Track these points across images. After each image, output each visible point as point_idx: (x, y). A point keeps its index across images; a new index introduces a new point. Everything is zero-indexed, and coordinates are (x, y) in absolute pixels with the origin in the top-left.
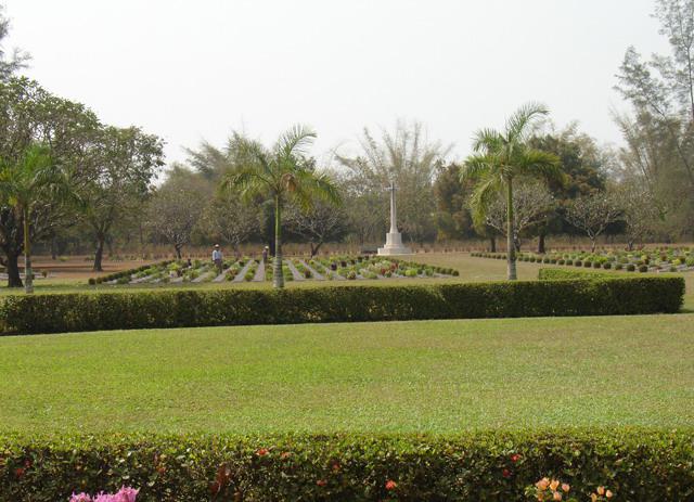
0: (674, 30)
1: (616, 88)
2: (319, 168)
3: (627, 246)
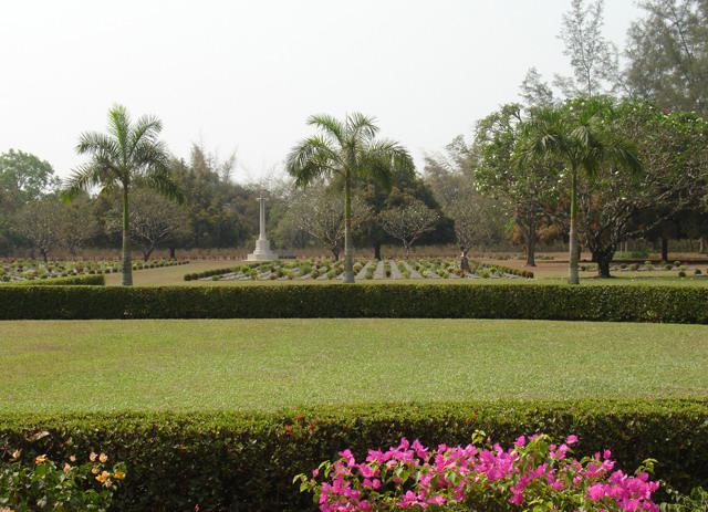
0: (577, 52)
1: (520, 95)
2: (420, 168)
3: (598, 455)
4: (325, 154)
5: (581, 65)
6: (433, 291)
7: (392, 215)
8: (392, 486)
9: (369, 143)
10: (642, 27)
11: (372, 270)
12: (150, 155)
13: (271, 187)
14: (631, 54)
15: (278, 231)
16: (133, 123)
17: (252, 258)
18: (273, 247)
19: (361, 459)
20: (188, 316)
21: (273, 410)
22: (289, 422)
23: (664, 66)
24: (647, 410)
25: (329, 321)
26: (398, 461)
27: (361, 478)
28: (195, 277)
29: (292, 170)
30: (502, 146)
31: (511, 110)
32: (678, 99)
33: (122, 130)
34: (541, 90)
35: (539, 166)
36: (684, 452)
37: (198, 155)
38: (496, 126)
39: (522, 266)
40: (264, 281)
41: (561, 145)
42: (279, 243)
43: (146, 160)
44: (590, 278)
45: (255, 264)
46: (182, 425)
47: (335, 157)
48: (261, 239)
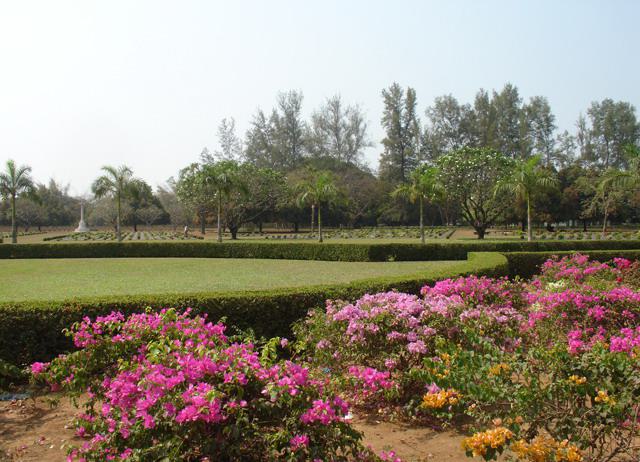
2: (155, 191)
4: (109, 183)
5: (226, 147)
6: (156, 246)
7: (142, 211)
8: (107, 332)
9: (130, 179)
10: (491, 98)
11: (131, 236)
12: (26, 183)
13: (87, 198)
14: (247, 143)
15: (90, 218)
16: (18, 168)
17: (77, 231)
18: (87, 225)
19: (93, 321)
20: (42, 258)
21: (63, 300)
22: (68, 305)
23: (260, 149)
24: (230, 296)
25: (108, 259)
26: (110, 321)
27: (93, 329)
28: (49, 239)
29: (94, 190)
30: (190, 181)
31: (195, 166)
32: (267, 163)
33: (12, 171)
34: (209, 157)
35: (206, 190)
36: (245, 313)
37: (53, 183)
38: (188, 172)
39: (199, 234)
40: (81, 241)
41: (214, 181)
42: (90, 224)
43: (23, 185)
44: (227, 239)
45: (79, 233)
46: (16, 307)
47: (113, 185)
48: (81, 222)
